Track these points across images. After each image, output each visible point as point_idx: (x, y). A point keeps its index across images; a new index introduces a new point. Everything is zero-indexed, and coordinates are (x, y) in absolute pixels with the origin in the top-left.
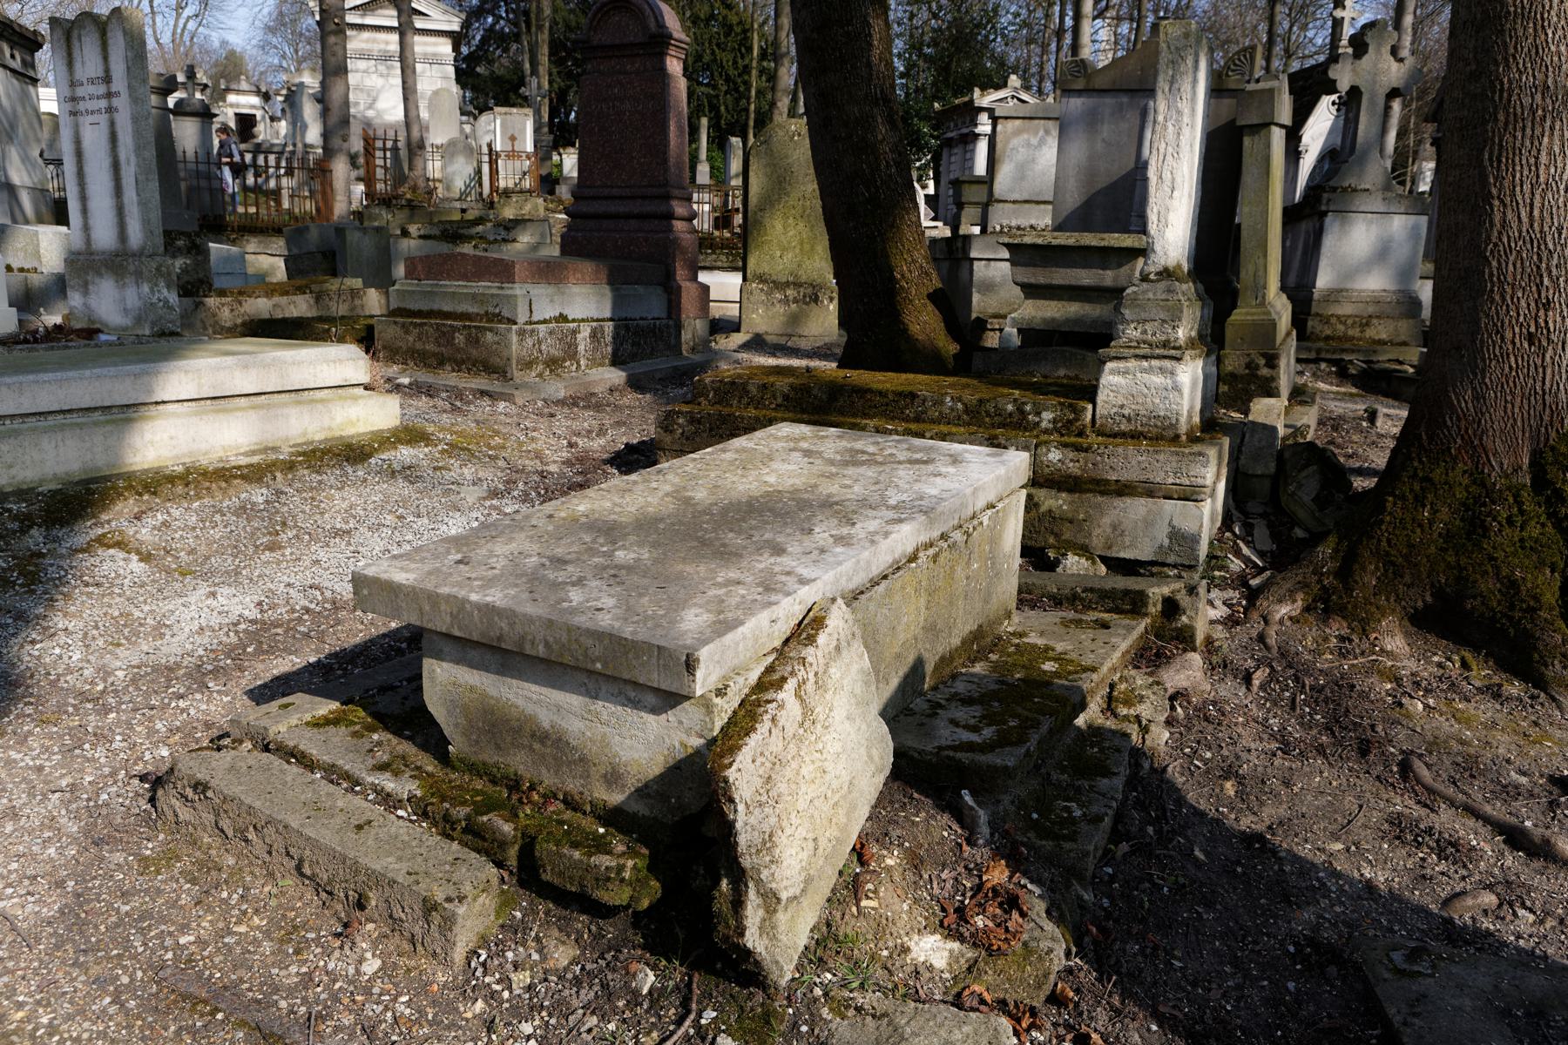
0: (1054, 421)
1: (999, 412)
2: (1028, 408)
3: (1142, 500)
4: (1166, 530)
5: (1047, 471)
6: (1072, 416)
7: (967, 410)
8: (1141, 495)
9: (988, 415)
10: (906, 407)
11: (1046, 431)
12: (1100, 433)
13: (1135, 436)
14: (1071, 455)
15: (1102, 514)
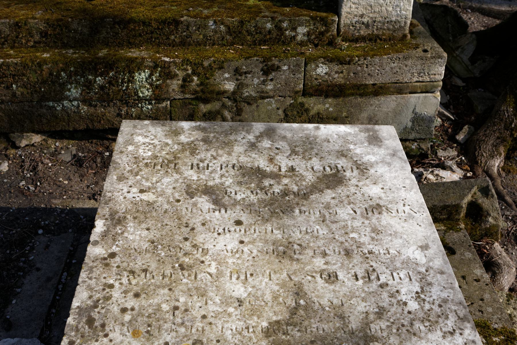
0: (308, 34)
1: (259, 30)
2: (285, 25)
3: (393, 97)
4: (410, 116)
5: (316, 82)
6: (323, 29)
7: (229, 31)
8: (392, 93)
9: (249, 33)
10: (171, 33)
11: (302, 44)
12: (345, 40)
13: (372, 39)
14: (336, 68)
15: (361, 111)
